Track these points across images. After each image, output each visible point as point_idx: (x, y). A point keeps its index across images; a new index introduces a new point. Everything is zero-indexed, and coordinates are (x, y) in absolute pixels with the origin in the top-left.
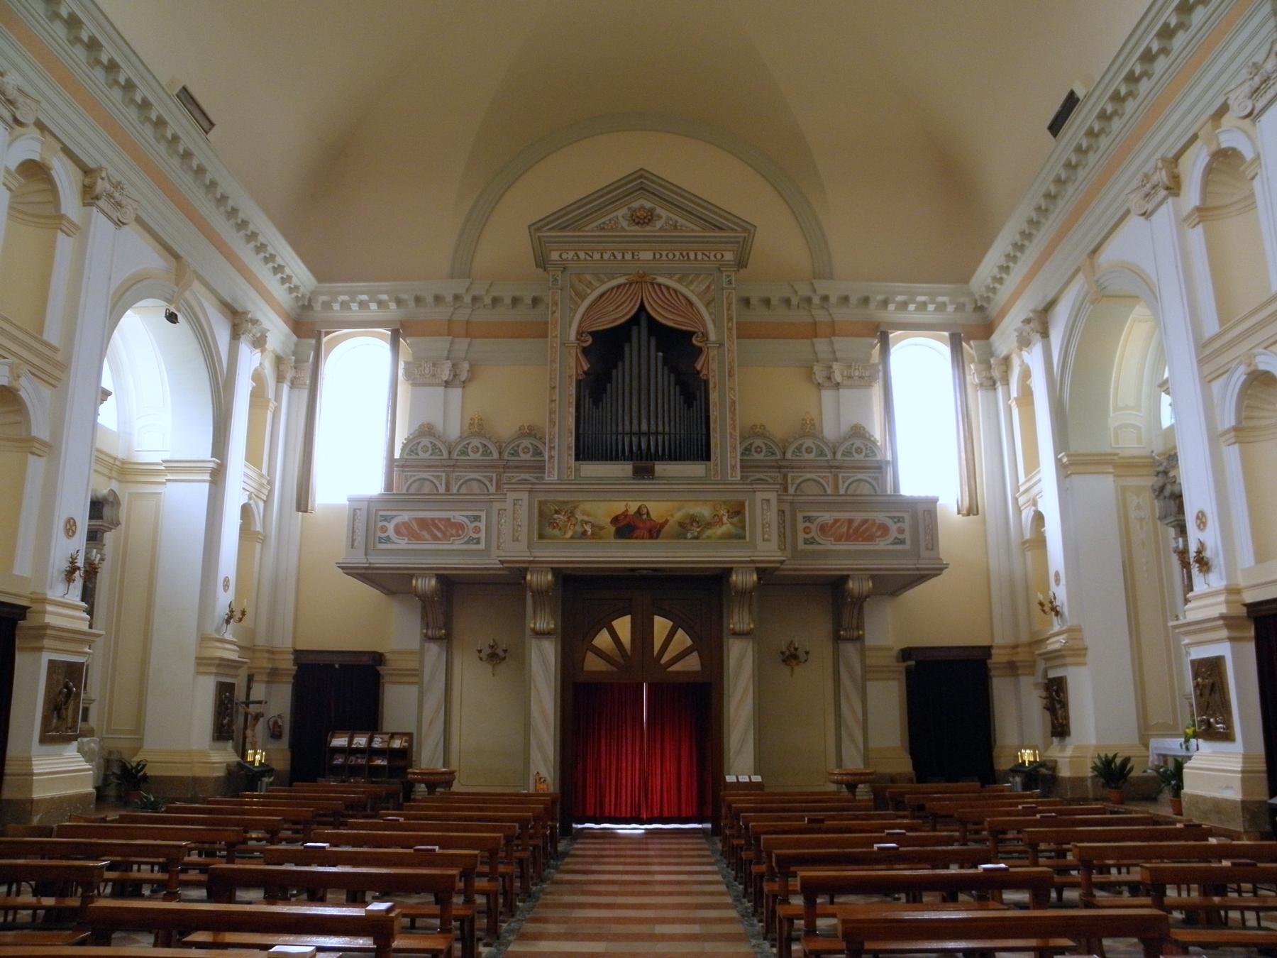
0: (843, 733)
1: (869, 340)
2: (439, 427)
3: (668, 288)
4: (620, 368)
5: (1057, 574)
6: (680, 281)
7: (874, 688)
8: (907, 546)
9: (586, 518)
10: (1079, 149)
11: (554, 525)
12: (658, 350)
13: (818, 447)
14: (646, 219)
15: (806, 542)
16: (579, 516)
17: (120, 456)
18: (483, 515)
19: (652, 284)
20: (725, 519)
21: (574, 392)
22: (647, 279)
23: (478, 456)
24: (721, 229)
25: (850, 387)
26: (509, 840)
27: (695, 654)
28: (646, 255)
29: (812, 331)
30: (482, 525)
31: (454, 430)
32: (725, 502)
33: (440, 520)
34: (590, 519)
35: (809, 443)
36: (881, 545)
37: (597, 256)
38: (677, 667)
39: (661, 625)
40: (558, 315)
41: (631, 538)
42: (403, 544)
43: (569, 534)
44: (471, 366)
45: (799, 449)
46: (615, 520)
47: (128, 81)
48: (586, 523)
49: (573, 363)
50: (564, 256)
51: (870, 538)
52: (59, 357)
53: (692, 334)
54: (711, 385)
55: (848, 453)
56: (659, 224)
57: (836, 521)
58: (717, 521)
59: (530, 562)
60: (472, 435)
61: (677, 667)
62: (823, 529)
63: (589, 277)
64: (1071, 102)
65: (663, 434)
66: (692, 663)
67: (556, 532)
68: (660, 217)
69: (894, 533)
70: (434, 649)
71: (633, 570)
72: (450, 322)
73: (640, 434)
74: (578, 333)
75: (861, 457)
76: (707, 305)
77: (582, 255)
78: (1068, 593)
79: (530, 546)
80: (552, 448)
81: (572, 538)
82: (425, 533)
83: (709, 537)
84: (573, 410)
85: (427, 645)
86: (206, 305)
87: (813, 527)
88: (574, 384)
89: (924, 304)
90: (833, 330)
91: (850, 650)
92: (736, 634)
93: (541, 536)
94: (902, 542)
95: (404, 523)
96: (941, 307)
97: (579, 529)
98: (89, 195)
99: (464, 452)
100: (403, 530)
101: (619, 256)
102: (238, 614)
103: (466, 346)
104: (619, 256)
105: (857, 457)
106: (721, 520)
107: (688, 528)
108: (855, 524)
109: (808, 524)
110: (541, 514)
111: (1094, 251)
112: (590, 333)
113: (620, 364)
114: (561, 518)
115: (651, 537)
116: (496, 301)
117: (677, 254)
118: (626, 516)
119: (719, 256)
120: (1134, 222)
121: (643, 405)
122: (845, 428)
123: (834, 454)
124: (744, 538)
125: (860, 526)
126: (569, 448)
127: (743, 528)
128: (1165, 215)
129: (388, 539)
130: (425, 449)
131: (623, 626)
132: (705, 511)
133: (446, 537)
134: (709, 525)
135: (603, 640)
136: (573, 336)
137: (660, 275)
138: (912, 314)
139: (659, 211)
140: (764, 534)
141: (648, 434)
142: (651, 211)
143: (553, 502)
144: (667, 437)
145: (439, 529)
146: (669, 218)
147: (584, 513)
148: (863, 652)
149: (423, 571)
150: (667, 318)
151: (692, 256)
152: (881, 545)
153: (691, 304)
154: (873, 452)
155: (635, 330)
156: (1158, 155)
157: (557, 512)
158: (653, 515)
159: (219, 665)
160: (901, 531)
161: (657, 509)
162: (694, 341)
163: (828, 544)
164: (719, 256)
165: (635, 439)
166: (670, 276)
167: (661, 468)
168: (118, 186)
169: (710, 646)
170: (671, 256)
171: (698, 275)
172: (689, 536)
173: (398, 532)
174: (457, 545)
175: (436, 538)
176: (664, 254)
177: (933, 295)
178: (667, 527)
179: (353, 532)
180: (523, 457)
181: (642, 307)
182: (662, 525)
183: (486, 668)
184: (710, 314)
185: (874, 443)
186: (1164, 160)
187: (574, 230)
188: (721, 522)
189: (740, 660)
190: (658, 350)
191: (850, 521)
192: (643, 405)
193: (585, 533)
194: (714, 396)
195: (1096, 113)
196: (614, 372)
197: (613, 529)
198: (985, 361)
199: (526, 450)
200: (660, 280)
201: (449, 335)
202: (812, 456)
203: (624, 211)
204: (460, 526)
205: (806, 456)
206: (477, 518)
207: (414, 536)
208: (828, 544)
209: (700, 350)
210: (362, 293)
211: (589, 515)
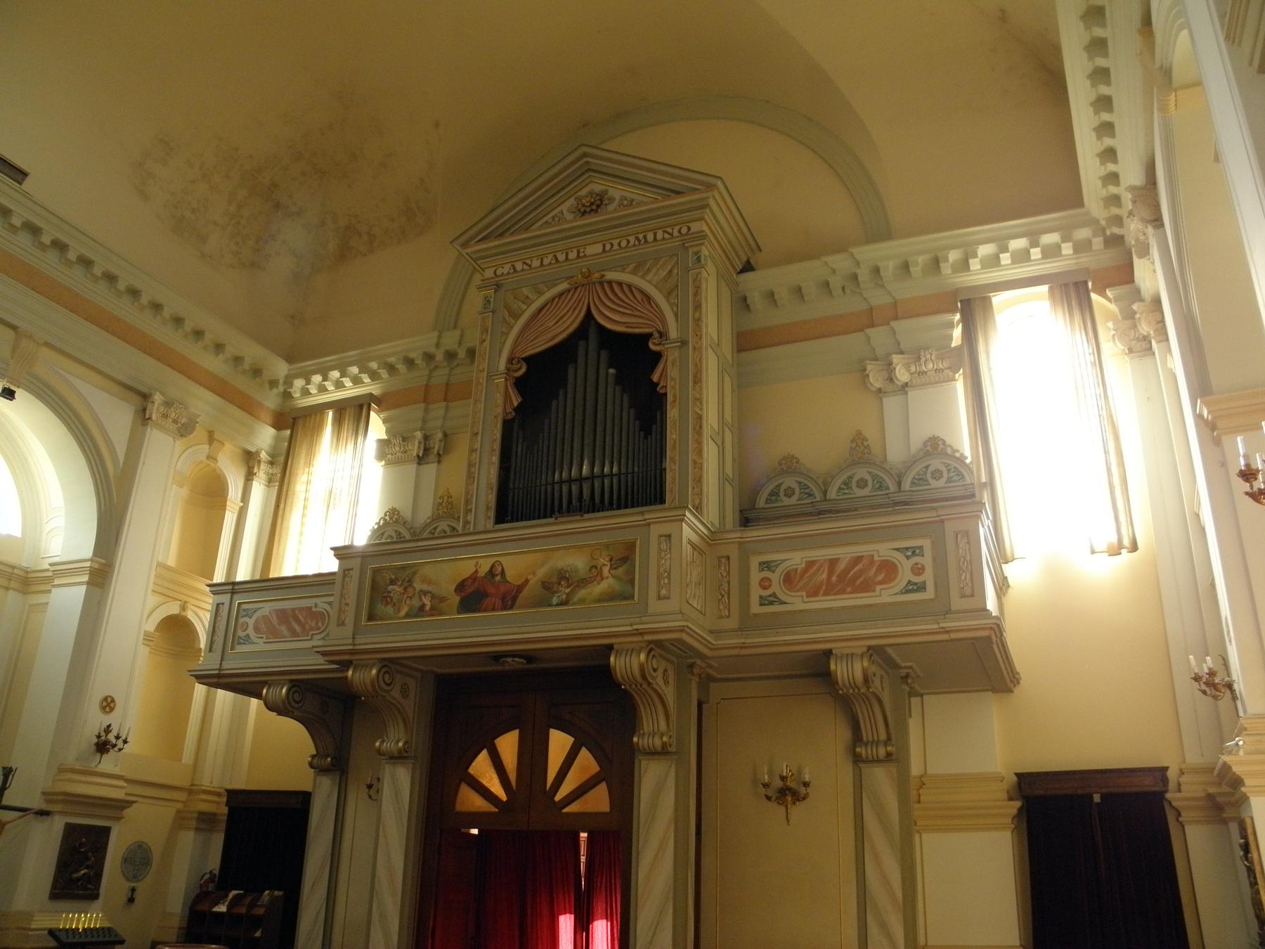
0: (870, 918)
1: (948, 317)
3: (620, 284)
4: (561, 397)
6: (634, 272)
7: (935, 849)
8: (929, 594)
9: (425, 587)
11: (387, 600)
13: (874, 477)
14: (597, 204)
15: (764, 601)
16: (418, 585)
17: (25, 564)
19: (601, 283)
20: (606, 570)
24: (678, 193)
27: (603, 787)
28: (590, 250)
29: (869, 319)
32: (607, 546)
33: (302, 609)
34: (430, 589)
35: (861, 473)
36: (886, 595)
39: (559, 742)
40: (487, 344)
44: (445, 435)
45: (847, 484)
46: (461, 587)
48: (426, 593)
49: (499, 399)
51: (866, 587)
55: (920, 480)
57: (810, 564)
58: (595, 572)
59: (352, 652)
62: (789, 579)
63: (525, 291)
66: (598, 801)
67: (390, 610)
68: (612, 200)
69: (905, 575)
71: (497, 657)
72: (427, 387)
73: (581, 479)
76: (668, 296)
77: (519, 266)
78: (884, 605)
80: (468, 511)
82: (283, 628)
83: (582, 601)
85: (319, 778)
86: (77, 383)
88: (499, 425)
89: (1026, 253)
90: (896, 312)
91: (880, 778)
92: (652, 753)
93: (371, 617)
94: (921, 587)
96: (1051, 252)
101: (561, 257)
103: (441, 412)
105: (934, 484)
107: (559, 587)
108: (842, 566)
109: (766, 574)
112: (525, 359)
114: (396, 589)
117: (632, 239)
122: (917, 442)
123: (899, 484)
124: (632, 597)
125: (847, 570)
126: (488, 508)
127: (632, 582)
131: (508, 745)
132: (577, 562)
134: (583, 582)
136: (502, 365)
137: (610, 270)
138: (1008, 269)
140: (659, 587)
145: (298, 622)
148: (902, 782)
150: (615, 320)
151: (650, 237)
153: (648, 298)
154: (960, 474)
155: (582, 343)
157: (392, 582)
158: (509, 575)
159: (65, 802)
160: (918, 570)
162: (652, 347)
163: (797, 602)
164: (684, 230)
169: (619, 773)
172: (555, 600)
173: (257, 629)
176: (615, 242)
178: (525, 593)
182: (520, 588)
184: (671, 305)
185: (961, 460)
189: (659, 791)
190: (610, 366)
191: (833, 563)
193: (422, 608)
194: (672, 413)
200: (611, 276)
204: (320, 616)
205: (860, 493)
207: (273, 633)
208: (797, 602)
209: (658, 356)
211: (430, 583)
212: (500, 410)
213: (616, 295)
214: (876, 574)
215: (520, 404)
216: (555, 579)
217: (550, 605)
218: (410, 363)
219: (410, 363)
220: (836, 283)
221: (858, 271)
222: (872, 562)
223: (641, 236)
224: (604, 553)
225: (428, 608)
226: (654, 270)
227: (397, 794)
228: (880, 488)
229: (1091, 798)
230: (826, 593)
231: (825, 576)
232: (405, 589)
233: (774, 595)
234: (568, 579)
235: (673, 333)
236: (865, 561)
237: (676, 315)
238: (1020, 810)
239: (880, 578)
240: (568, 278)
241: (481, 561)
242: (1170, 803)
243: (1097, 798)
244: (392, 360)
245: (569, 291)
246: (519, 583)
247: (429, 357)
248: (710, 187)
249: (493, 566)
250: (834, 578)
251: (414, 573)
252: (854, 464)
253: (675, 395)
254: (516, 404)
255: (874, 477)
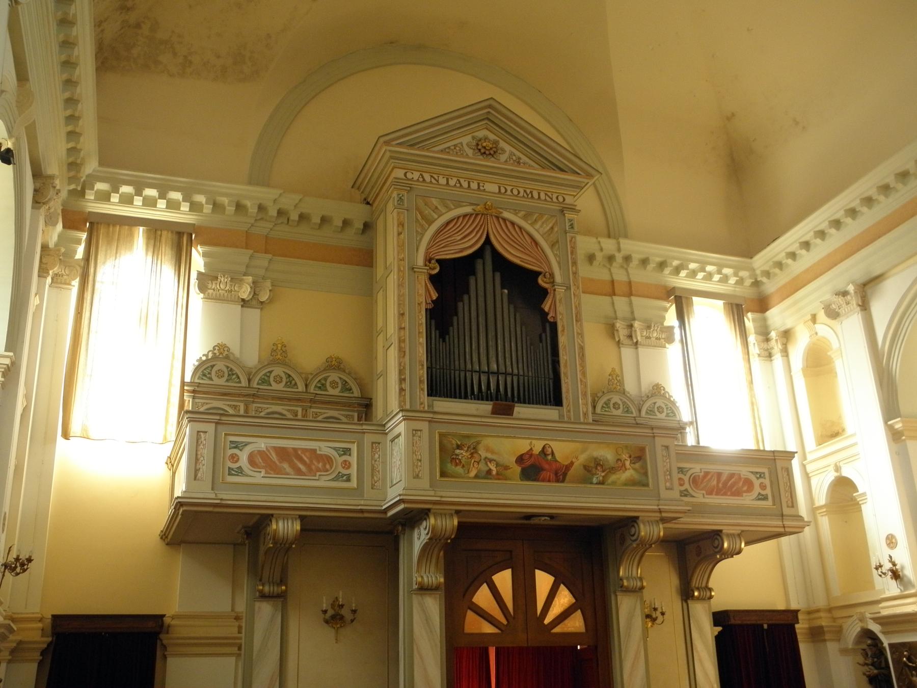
2: (235, 350)
3: (513, 224)
6: (525, 218)
9: (489, 456)
11: (456, 461)
12: (503, 287)
13: (624, 403)
16: (483, 453)
18: (354, 448)
19: (497, 218)
20: (628, 463)
21: (424, 321)
22: (494, 212)
23: (280, 387)
24: (562, 170)
25: (649, 346)
27: (579, 612)
28: (493, 188)
30: (353, 459)
31: (251, 357)
32: (626, 447)
33: (305, 450)
36: (748, 500)
37: (443, 181)
38: (557, 630)
39: (543, 581)
41: (536, 480)
42: (258, 477)
43: (473, 473)
45: (607, 403)
46: (520, 460)
48: (491, 461)
49: (422, 291)
50: (409, 176)
51: (738, 493)
53: (538, 274)
54: (560, 328)
55: (650, 412)
56: (503, 158)
58: (619, 466)
60: (274, 362)
61: (557, 630)
62: (695, 481)
63: (435, 202)
65: (512, 374)
66: (576, 623)
67: (459, 470)
68: (504, 151)
70: (265, 610)
71: (529, 517)
72: (248, 234)
74: (426, 260)
75: (663, 416)
76: (552, 246)
77: (427, 177)
79: (432, 485)
81: (476, 477)
82: (286, 466)
83: (614, 483)
84: (423, 340)
87: (686, 478)
88: (424, 312)
90: (630, 291)
93: (443, 474)
95: (261, 453)
97: (483, 467)
99: (265, 381)
100: (259, 460)
104: (465, 185)
106: (624, 465)
107: (594, 471)
108: (724, 478)
110: (442, 448)
112: (438, 261)
113: (466, 297)
114: (463, 454)
115: (558, 481)
116: (303, 217)
117: (522, 191)
118: (531, 455)
119: (561, 199)
121: (491, 343)
122: (646, 386)
123: (640, 411)
124: (647, 485)
126: (421, 382)
127: (646, 474)
129: (240, 471)
130: (220, 374)
131: (504, 579)
132: (607, 454)
133: (311, 471)
134: (612, 470)
135: (483, 597)
136: (420, 261)
137: (506, 209)
139: (502, 144)
141: (497, 373)
142: (496, 143)
143: (454, 435)
144: (515, 379)
146: (512, 154)
147: (487, 449)
149: (285, 511)
152: (748, 500)
153: (536, 243)
154: (673, 412)
157: (459, 447)
158: (558, 456)
160: (763, 487)
161: (562, 450)
164: (561, 199)
165: (484, 378)
166: (516, 212)
167: (521, 410)
169: (596, 602)
170: (515, 192)
171: (541, 215)
172: (595, 480)
173: (252, 461)
174: (324, 482)
175: (299, 472)
177: (720, 267)
179: (197, 459)
180: (331, 391)
181: (488, 241)
182: (568, 467)
183: (328, 633)
184: (555, 255)
187: (422, 148)
188: (623, 467)
190: (503, 287)
191: (719, 475)
192: (491, 343)
193: (489, 472)
196: (460, 304)
197: (518, 469)
198: (764, 333)
199: (334, 385)
200: (506, 215)
201: (247, 247)
202: (619, 412)
203: (467, 139)
204: (328, 459)
205: (615, 412)
206: (347, 452)
208: (700, 497)
210: (151, 186)
211: (493, 452)
212: (423, 299)
213: (509, 230)
214: (743, 486)
215: (437, 298)
216: (592, 465)
217: (591, 483)
218: (239, 207)
219: (239, 207)
220: (599, 256)
221: (617, 254)
222: (740, 478)
223: (528, 191)
224: (625, 451)
225: (494, 473)
226: (540, 223)
227: (427, 620)
228: (627, 412)
229: (762, 626)
230: (717, 494)
231: (715, 482)
232: (472, 454)
233: (686, 490)
234: (602, 466)
235: (558, 278)
236: (736, 477)
237: (559, 263)
238: (49, 645)
239: (745, 488)
240: (472, 204)
241: (534, 442)
242: (161, 640)
243: (765, 626)
244: (225, 200)
245: (471, 215)
246: (566, 463)
247: (261, 208)
248: (589, 176)
249: (544, 447)
250: (720, 485)
251: (478, 443)
252: (610, 391)
253: (563, 326)
254: (434, 298)
255: (624, 403)
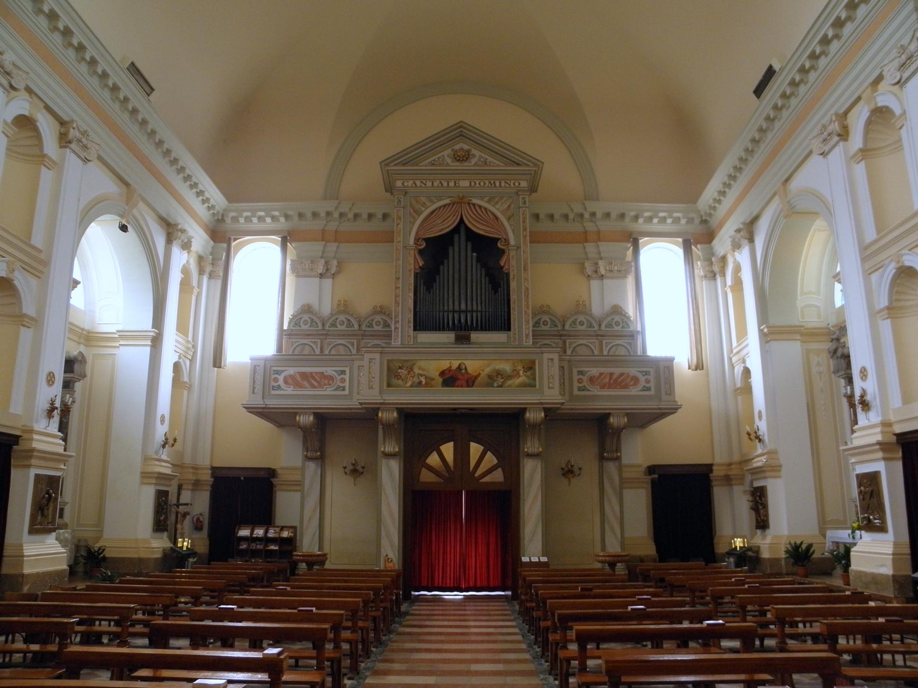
0: (606, 526)
1: (625, 244)
2: (316, 307)
3: (480, 207)
4: (446, 265)
5: (760, 412)
6: (489, 202)
7: (628, 494)
8: (652, 392)
9: (421, 372)
10: (775, 107)
11: (398, 377)
12: (473, 251)
13: (588, 321)
14: (464, 157)
15: (580, 389)
16: (416, 371)
17: (87, 327)
18: (347, 370)
19: (469, 204)
20: (521, 373)
21: (413, 281)
22: (465, 200)
23: (343, 328)
24: (518, 164)
25: (611, 278)
26: (366, 603)
27: (500, 470)
28: (465, 183)
29: (584, 238)
30: (347, 377)
31: (326, 309)
32: (521, 361)
33: (316, 373)
34: (424, 373)
35: (581, 318)
36: (634, 391)
37: (429, 184)
38: (486, 479)
39: (475, 449)
40: (401, 226)
41: (453, 386)
42: (290, 391)
43: (409, 384)
44: (339, 263)
45: (574, 322)
46: (442, 374)
47: (92, 58)
48: (421, 375)
49: (412, 261)
50: (406, 184)
51: (626, 387)
52: (42, 256)
53: (497, 240)
54: (511, 277)
55: (609, 325)
56: (474, 161)
57: (601, 374)
58: (515, 374)
59: (381, 404)
60: (340, 312)
61: (486, 479)
62: (592, 380)
63: (423, 199)
64: (770, 73)
65: (477, 311)
66: (498, 476)
67: (400, 382)
68: (474, 156)
69: (643, 383)
70: (312, 466)
71: (455, 409)
72: (323, 231)
73: (460, 311)
74: (415, 239)
75: (619, 328)
76: (509, 219)
77: (418, 183)
78: (768, 426)
79: (381, 392)
80: (397, 322)
81: (411, 386)
82: (305, 383)
83: (510, 386)
84: (412, 294)
85: (307, 463)
86: (148, 219)
87: (585, 378)
88: (413, 276)
89: (665, 219)
90: (599, 237)
91: (611, 467)
92: (529, 455)
93: (389, 385)
94: (649, 389)
95: (290, 376)
96: (677, 221)
97: (416, 380)
98: (64, 140)
99: (333, 325)
100: (290, 381)
101: (445, 184)
102: (171, 441)
103: (335, 249)
104: (445, 184)
105: (616, 328)
106: (518, 373)
107: (495, 379)
108: (615, 377)
109: (581, 376)
110: (389, 369)
111: (787, 180)
112: (424, 239)
113: (446, 261)
114: (403, 372)
115: (468, 386)
116: (356, 216)
117: (487, 182)
118: (450, 371)
119: (517, 184)
120: (815, 159)
121: (463, 291)
122: (607, 307)
123: (600, 326)
124: (535, 386)
125: (618, 378)
126: (409, 322)
127: (534, 379)
128: (838, 154)
129: (279, 387)
130: (306, 323)
131: (448, 449)
132: (507, 367)
133: (321, 385)
134: (510, 377)
135: (433, 459)
136: (412, 241)
137: (474, 197)
138: (655, 226)
139: (474, 151)
140: (549, 383)
141: (466, 312)
142: (468, 151)
143: (398, 360)
144: (479, 314)
145: (315, 380)
146: (481, 157)
147: (420, 368)
148: (620, 468)
149: (304, 410)
150: (479, 229)
151: (497, 184)
152: (634, 391)
153: (497, 218)
154: (628, 324)
155: (456, 237)
156: (832, 111)
157: (400, 368)
158: (470, 370)
159: (157, 478)
160: (648, 381)
161: (472, 366)
162: (499, 245)
163: (595, 391)
164: (517, 184)
165: (456, 316)
166: (482, 198)
167: (475, 336)
168: (85, 133)
169: (511, 464)
170: (482, 184)
171: (502, 198)
172: (495, 385)
173: (286, 382)
174: (329, 391)
175: (313, 386)
176: (477, 182)
177: (670, 212)
178: (479, 379)
179: (254, 382)
180: (376, 328)
181: (462, 221)
182: (476, 377)
183: (350, 479)
184: (511, 225)
185: (628, 318)
186: (836, 115)
187: (413, 165)
188: (518, 375)
189: (532, 474)
190: (473, 251)
191: (611, 374)
192: (463, 291)
193: (420, 383)
194: (513, 285)
195: (788, 81)
196: (441, 267)
197: (440, 380)
198: (708, 259)
199: (378, 323)
200: (475, 201)
201: (323, 240)
202: (583, 328)
203: (449, 151)
204: (331, 378)
205: (580, 328)
206: (343, 372)
207: (297, 385)
208: (595, 391)
209: (503, 252)
210: (260, 211)
211: (423, 370)
